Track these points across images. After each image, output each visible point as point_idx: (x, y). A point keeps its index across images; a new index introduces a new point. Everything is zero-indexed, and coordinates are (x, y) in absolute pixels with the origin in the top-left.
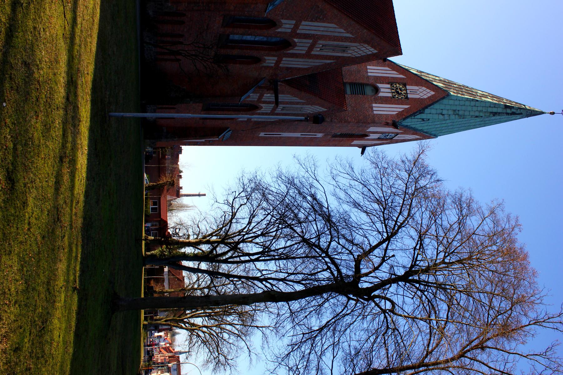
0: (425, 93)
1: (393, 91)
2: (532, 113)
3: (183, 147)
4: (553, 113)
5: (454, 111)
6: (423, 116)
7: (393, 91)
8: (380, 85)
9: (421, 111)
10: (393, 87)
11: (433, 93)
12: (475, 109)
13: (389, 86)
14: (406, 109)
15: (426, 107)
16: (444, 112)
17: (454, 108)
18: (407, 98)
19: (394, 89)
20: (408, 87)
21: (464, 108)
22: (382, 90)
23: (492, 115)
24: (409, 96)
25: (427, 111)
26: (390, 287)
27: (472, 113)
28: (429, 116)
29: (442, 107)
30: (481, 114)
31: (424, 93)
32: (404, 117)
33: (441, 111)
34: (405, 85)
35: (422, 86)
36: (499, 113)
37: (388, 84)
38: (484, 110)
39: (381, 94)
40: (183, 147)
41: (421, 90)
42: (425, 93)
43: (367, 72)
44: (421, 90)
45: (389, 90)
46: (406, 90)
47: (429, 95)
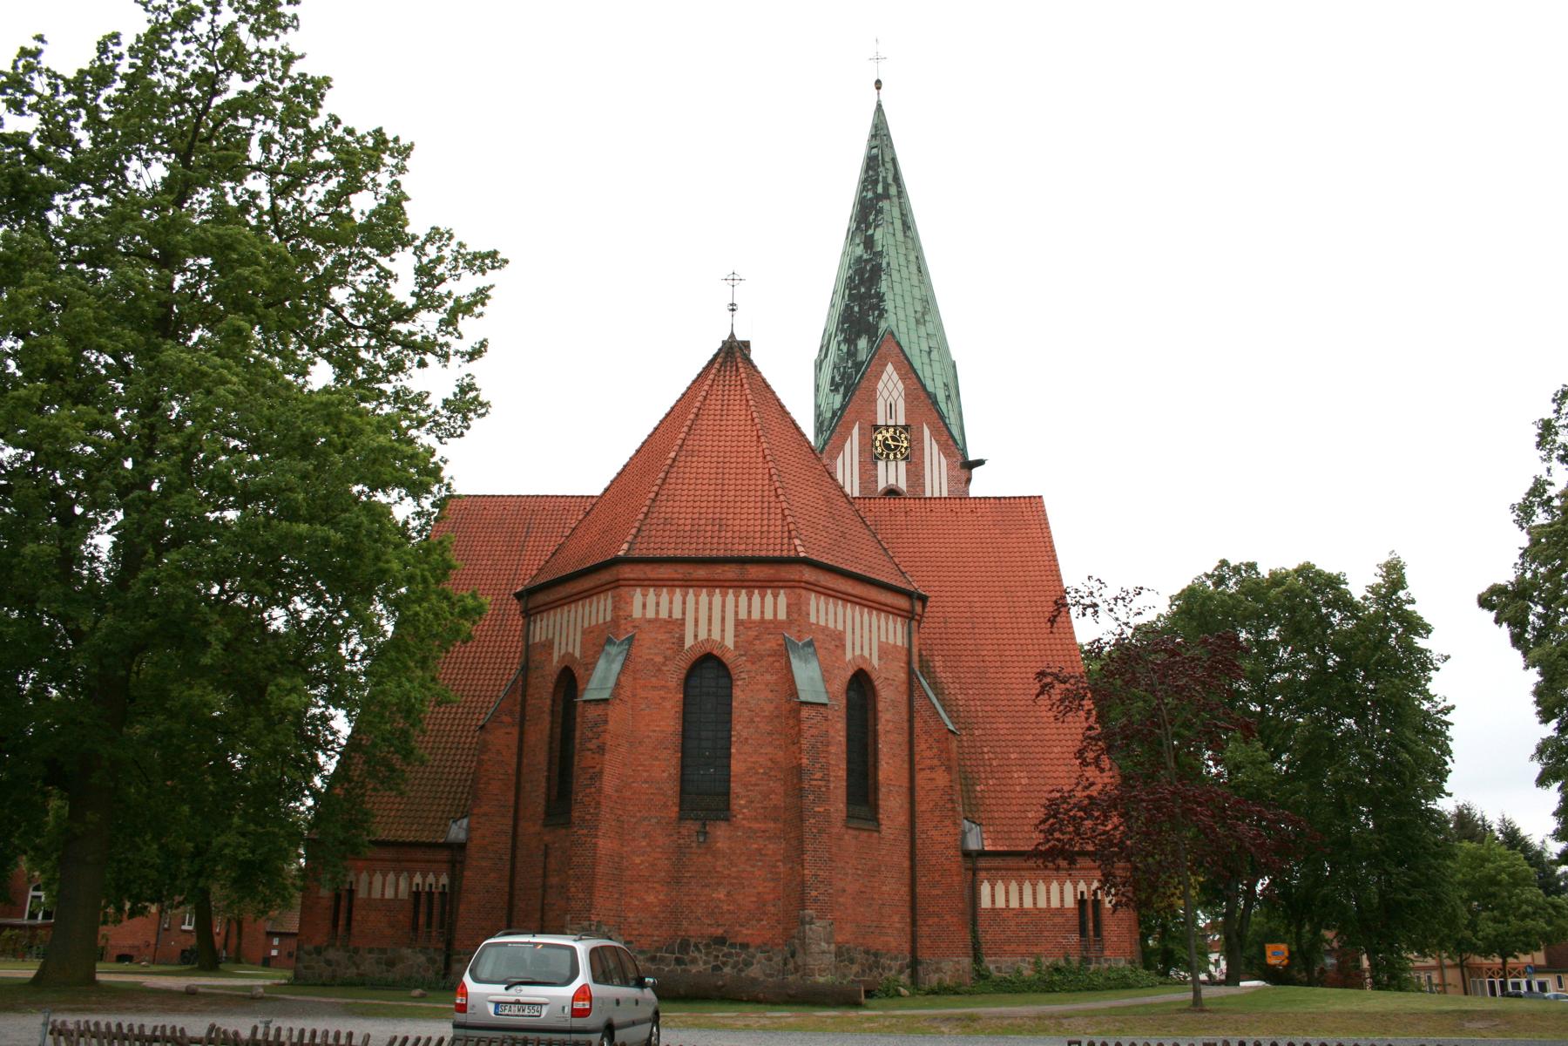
0: (890, 385)
1: (891, 456)
2: (880, 133)
3: (1540, 679)
4: (878, 85)
5: (917, 322)
6: (941, 397)
7: (891, 456)
8: (881, 485)
9: (932, 399)
10: (882, 454)
11: (890, 368)
12: (904, 270)
13: (881, 464)
14: (932, 434)
15: (924, 387)
16: (925, 347)
17: (912, 321)
18: (906, 428)
19: (888, 455)
20: (881, 422)
21: (908, 299)
22: (892, 481)
23: (909, 233)
24: (902, 421)
25: (930, 388)
26: (1039, 844)
27: (915, 281)
28: (939, 384)
29: (916, 351)
30: (912, 258)
31: (594, 501)
32: (951, 442)
33: (925, 355)
34: (876, 428)
35: (875, 390)
36: (902, 214)
37: (876, 464)
38: (902, 251)
39: (903, 485)
40: (1540, 679)
41: (886, 394)
42: (890, 385)
43: (597, 625)
44: (886, 394)
45: (892, 465)
46: (887, 427)
47: (895, 377)
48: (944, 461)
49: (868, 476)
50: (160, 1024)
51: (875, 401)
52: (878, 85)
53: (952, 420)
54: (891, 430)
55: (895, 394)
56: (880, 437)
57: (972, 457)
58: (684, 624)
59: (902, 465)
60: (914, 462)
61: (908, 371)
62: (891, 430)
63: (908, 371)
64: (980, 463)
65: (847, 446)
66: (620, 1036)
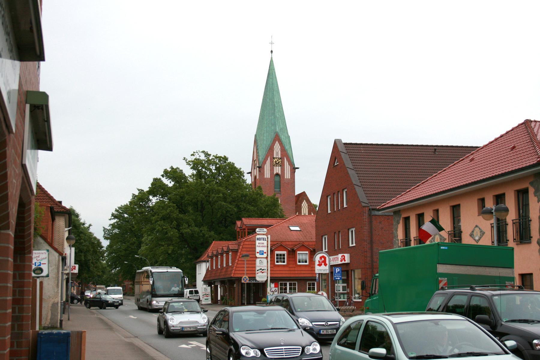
4: (272, 52)
8: (275, 173)
11: (305, 201)
18: (280, 158)
20: (275, 157)
22: (277, 172)
24: (280, 157)
34: (274, 158)
39: (280, 173)
41: (276, 149)
46: (276, 158)
48: (289, 167)
49: (272, 170)
50: (34, 200)
51: (301, 208)
52: (272, 52)
53: (289, 152)
54: (277, 159)
55: (278, 149)
56: (274, 160)
57: (296, 167)
58: (355, 345)
59: (280, 167)
60: (282, 165)
61: (281, 144)
62: (277, 159)
63: (281, 144)
64: (298, 168)
65: (267, 162)
66: (46, 123)
